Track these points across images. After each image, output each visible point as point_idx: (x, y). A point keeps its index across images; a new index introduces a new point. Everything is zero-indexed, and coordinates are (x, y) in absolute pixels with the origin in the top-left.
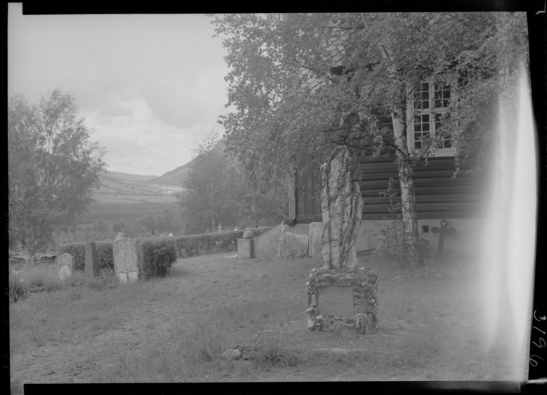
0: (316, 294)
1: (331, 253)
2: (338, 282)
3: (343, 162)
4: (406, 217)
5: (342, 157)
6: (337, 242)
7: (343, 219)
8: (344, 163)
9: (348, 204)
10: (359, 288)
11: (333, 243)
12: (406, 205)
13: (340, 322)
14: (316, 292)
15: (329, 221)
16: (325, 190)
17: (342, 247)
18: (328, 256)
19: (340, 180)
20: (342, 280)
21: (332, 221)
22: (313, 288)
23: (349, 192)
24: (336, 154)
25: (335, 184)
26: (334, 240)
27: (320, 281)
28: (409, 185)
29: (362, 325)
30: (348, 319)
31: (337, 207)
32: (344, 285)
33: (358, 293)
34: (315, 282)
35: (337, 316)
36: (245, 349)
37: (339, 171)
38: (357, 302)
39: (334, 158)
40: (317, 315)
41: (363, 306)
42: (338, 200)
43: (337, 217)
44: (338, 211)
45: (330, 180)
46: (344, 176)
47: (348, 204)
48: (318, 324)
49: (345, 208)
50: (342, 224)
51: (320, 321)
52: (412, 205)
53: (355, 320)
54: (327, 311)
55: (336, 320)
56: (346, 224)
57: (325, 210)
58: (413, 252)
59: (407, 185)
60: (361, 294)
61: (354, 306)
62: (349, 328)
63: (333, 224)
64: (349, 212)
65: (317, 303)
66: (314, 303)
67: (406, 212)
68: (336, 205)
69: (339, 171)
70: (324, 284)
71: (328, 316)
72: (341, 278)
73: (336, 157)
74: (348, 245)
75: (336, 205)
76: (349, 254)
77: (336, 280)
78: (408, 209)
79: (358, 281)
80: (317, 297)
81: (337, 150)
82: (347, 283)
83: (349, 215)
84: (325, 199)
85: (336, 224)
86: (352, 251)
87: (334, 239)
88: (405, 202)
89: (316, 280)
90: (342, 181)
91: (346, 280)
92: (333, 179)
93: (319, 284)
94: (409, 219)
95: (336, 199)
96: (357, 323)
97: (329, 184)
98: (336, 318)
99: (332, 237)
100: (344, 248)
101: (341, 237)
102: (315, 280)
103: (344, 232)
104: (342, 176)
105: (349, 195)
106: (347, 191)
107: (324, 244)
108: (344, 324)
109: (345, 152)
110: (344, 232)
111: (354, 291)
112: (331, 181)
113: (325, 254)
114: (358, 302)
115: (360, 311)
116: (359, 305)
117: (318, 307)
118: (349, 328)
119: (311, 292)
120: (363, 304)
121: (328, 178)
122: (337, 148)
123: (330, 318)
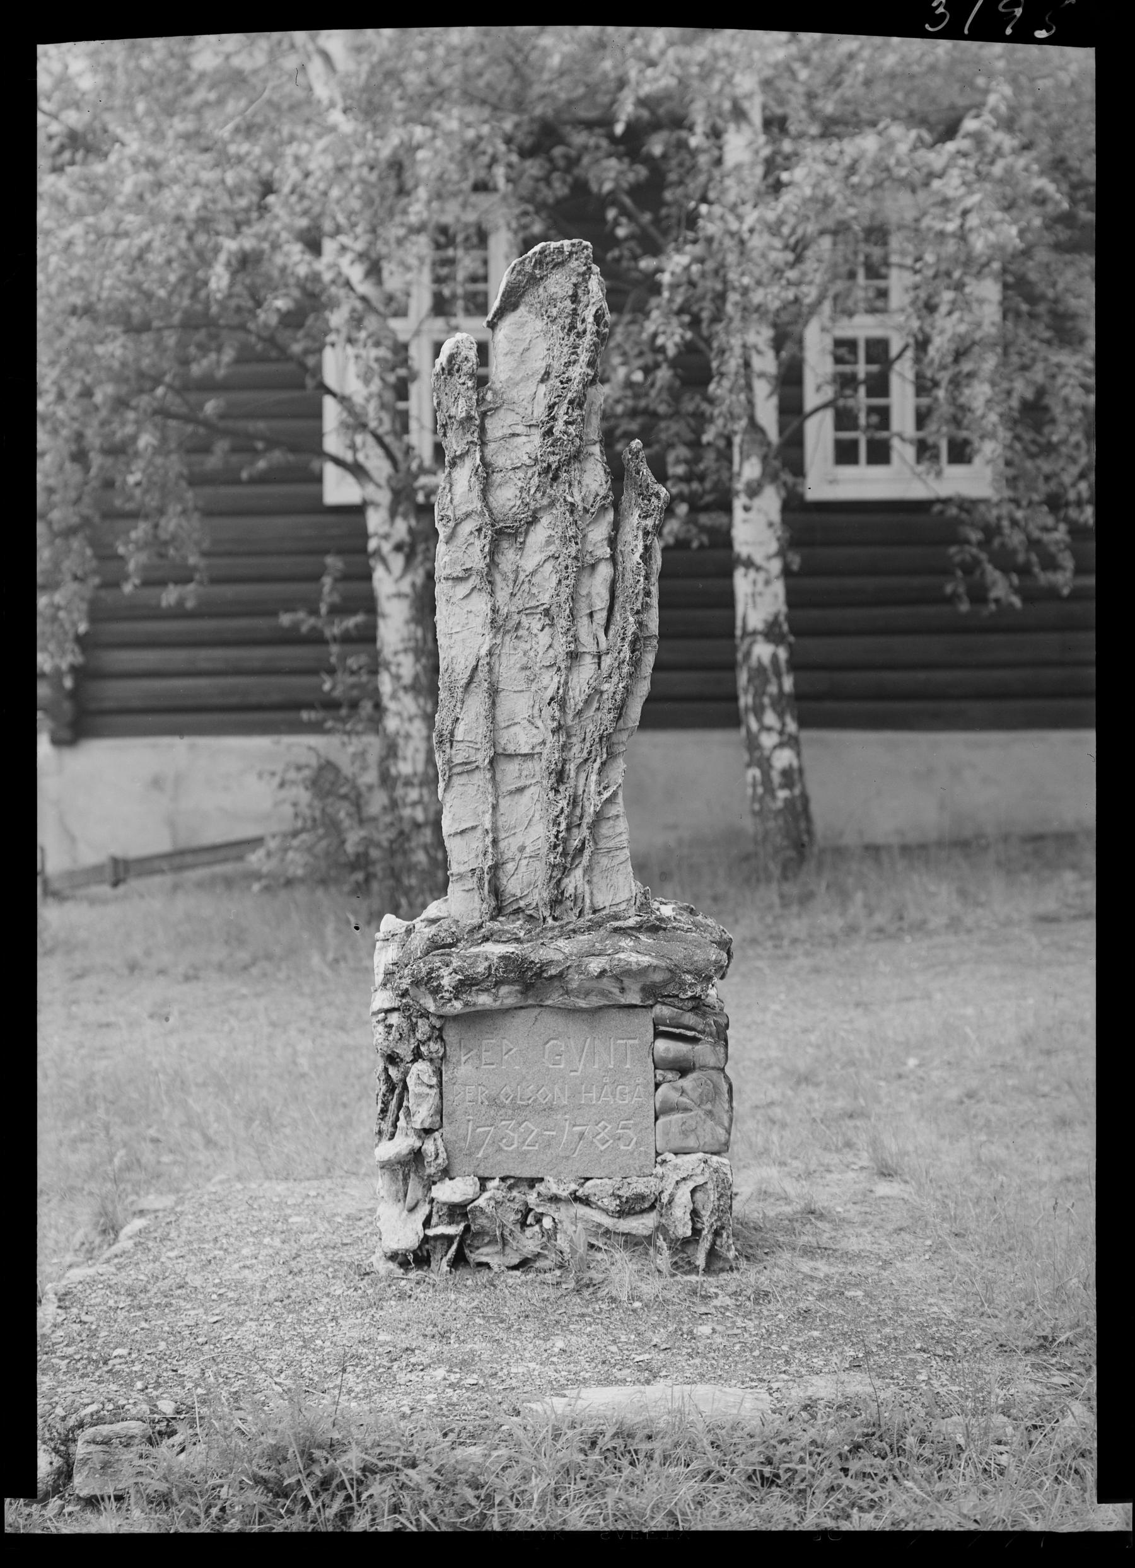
0: (431, 1060)
2: (574, 985)
3: (572, 327)
4: (399, 714)
5: (568, 302)
6: (537, 767)
7: (576, 639)
8: (580, 335)
9: (599, 560)
10: (690, 1019)
11: (510, 771)
12: (399, 665)
13: (581, 1210)
14: (434, 1046)
15: (490, 654)
16: (463, 477)
17: (566, 791)
18: (478, 842)
19: (559, 426)
20: (603, 973)
22: (413, 1028)
23: (602, 493)
24: (534, 281)
25: (531, 444)
26: (511, 756)
27: (466, 984)
28: (413, 585)
29: (707, 1221)
30: (625, 1193)
31: (533, 574)
32: (604, 1002)
33: (682, 1047)
35: (559, 1181)
37: (542, 381)
38: (675, 1097)
39: (515, 307)
41: (710, 1113)
42: (539, 535)
44: (545, 598)
45: (496, 427)
46: (580, 406)
47: (599, 560)
49: (585, 579)
50: (569, 669)
51: (457, 1211)
54: (500, 1149)
55: (555, 1199)
57: (463, 589)
58: (427, 852)
59: (405, 586)
61: (656, 1119)
62: (632, 1242)
63: (508, 671)
64: (601, 602)
66: (422, 1114)
68: (529, 562)
69: (542, 381)
70: (484, 1000)
71: (503, 1179)
73: (527, 299)
74: (599, 783)
75: (529, 564)
77: (560, 976)
78: (407, 679)
79: (688, 978)
81: (539, 263)
82: (623, 990)
83: (601, 617)
84: (468, 527)
85: (525, 668)
87: (511, 749)
88: (396, 653)
90: (572, 429)
91: (622, 976)
92: (511, 418)
93: (458, 1005)
95: (527, 533)
97: (491, 447)
98: (552, 1186)
99: (504, 737)
102: (439, 977)
103: (579, 713)
104: (571, 402)
106: (594, 487)
107: (456, 780)
108: (608, 1222)
111: (658, 1034)
112: (499, 434)
113: (463, 832)
114: (683, 1092)
115: (691, 1142)
116: (686, 1109)
118: (632, 1242)
119: (404, 1051)
120: (709, 1106)
121: (484, 415)
122: (542, 252)
123: (510, 1188)
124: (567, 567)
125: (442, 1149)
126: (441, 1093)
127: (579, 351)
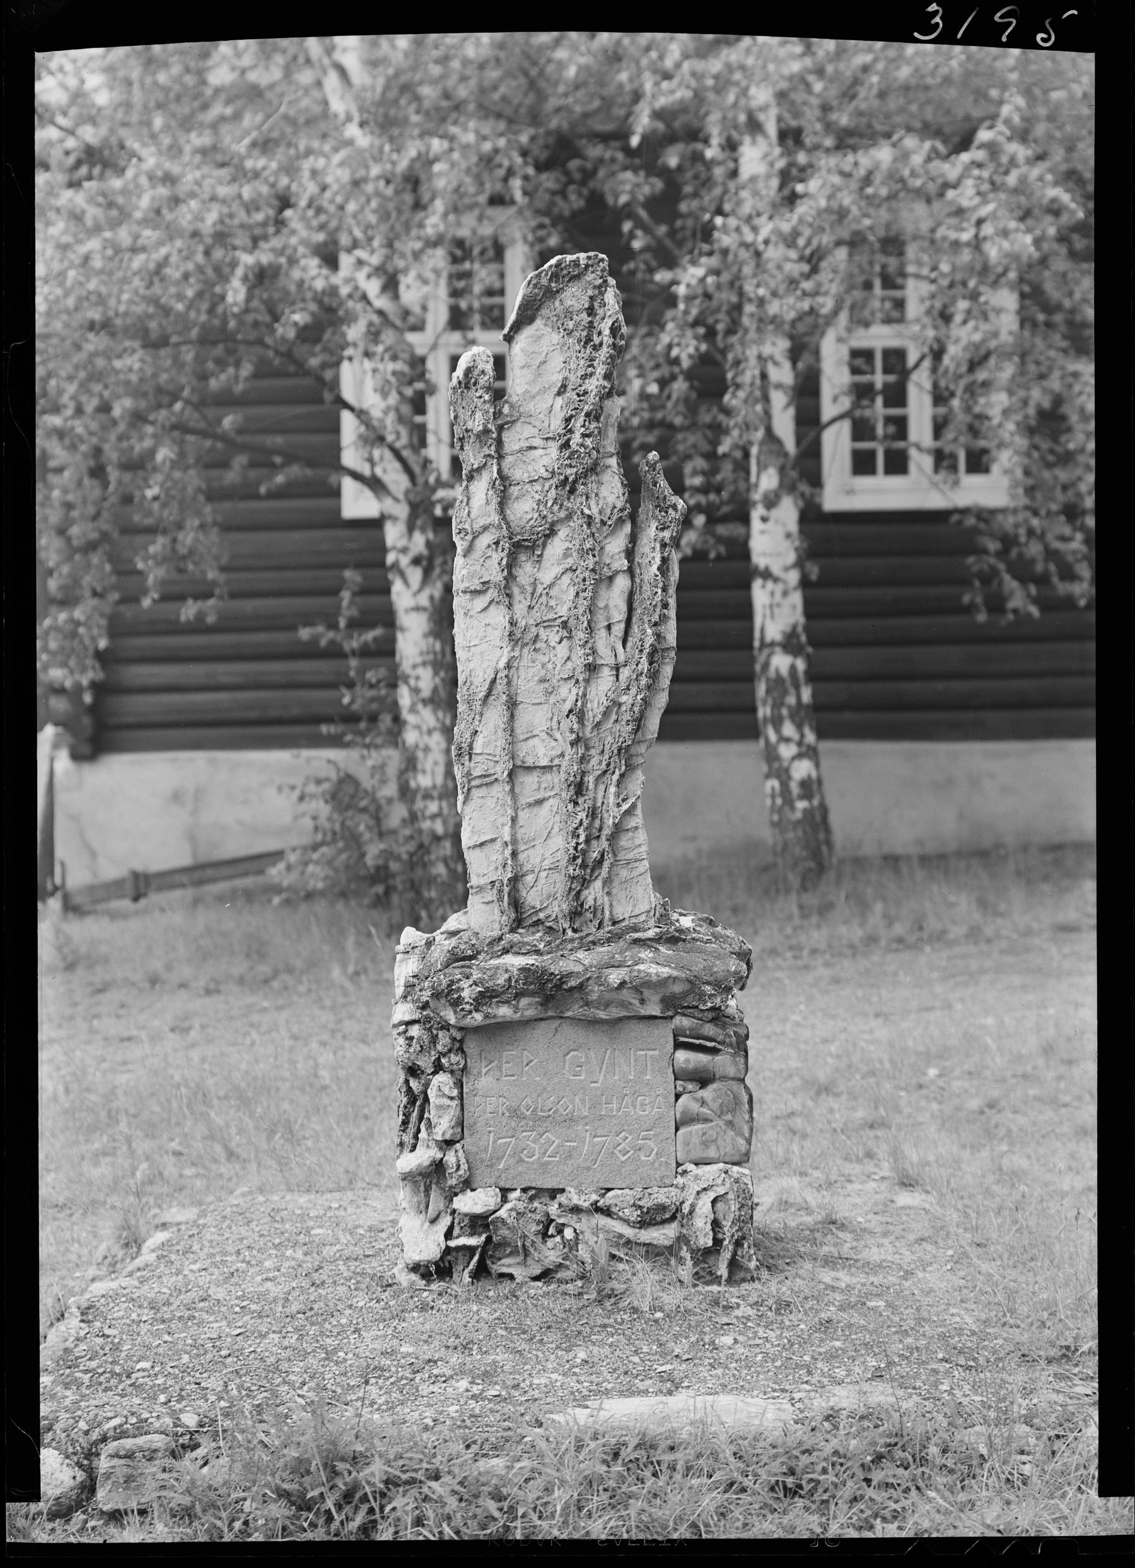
0: (452, 1072)
1: (514, 841)
2: (594, 997)
3: (589, 339)
4: (418, 727)
5: (584, 315)
7: (594, 652)
8: (596, 348)
9: (617, 572)
10: (709, 1029)
12: (418, 678)
13: (603, 1221)
14: (454, 1058)
15: (508, 666)
18: (497, 854)
19: (576, 439)
20: (623, 984)
21: (524, 663)
23: (619, 505)
27: (486, 997)
28: (432, 598)
29: (729, 1231)
30: (646, 1203)
31: (551, 586)
33: (702, 1058)
34: (456, 1003)
35: (580, 1192)
36: (112, 1446)
37: (559, 394)
38: (695, 1107)
39: (531, 320)
40: (463, 1191)
41: (730, 1124)
42: (556, 547)
43: (554, 638)
45: (513, 440)
46: (597, 418)
48: (473, 1241)
49: (603, 592)
50: (587, 681)
51: (478, 1222)
52: (443, 680)
53: (686, 1209)
54: (521, 1161)
55: (576, 1210)
56: (605, 682)
58: (447, 865)
60: (718, 1058)
61: (677, 1129)
62: (652, 1252)
63: (527, 683)
64: (618, 614)
65: (461, 1123)
66: (443, 1126)
67: (420, 707)
68: (547, 575)
69: (559, 394)
70: (504, 1012)
71: (524, 1190)
72: (614, 977)
73: (544, 312)
74: (618, 795)
75: (546, 577)
76: (624, 841)
77: (581, 987)
78: (426, 693)
80: (459, 1085)
81: (555, 276)
82: (642, 1001)
83: (619, 629)
85: (543, 681)
86: (636, 828)
87: (530, 762)
88: (414, 667)
89: (466, 994)
90: (589, 442)
91: (641, 987)
92: (528, 431)
93: (478, 1017)
94: (430, 732)
95: (544, 545)
96: (701, 1223)
97: (509, 460)
98: (574, 1197)
99: (523, 750)
100: (593, 813)
101: (581, 751)
102: (461, 989)
103: (598, 725)
104: (588, 415)
105: (620, 521)
106: (611, 499)
107: (475, 793)
108: (629, 1232)
109: (602, 288)
110: (598, 725)
111: (678, 1045)
113: (482, 844)
114: (703, 1103)
115: (712, 1153)
116: (707, 1120)
117: (468, 1140)
118: (652, 1252)
119: (425, 1063)
120: (729, 1117)
121: (500, 429)
122: (558, 265)
124: (584, 580)
125: (463, 1160)
126: (462, 1105)
127: (595, 363)
